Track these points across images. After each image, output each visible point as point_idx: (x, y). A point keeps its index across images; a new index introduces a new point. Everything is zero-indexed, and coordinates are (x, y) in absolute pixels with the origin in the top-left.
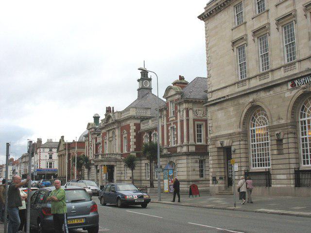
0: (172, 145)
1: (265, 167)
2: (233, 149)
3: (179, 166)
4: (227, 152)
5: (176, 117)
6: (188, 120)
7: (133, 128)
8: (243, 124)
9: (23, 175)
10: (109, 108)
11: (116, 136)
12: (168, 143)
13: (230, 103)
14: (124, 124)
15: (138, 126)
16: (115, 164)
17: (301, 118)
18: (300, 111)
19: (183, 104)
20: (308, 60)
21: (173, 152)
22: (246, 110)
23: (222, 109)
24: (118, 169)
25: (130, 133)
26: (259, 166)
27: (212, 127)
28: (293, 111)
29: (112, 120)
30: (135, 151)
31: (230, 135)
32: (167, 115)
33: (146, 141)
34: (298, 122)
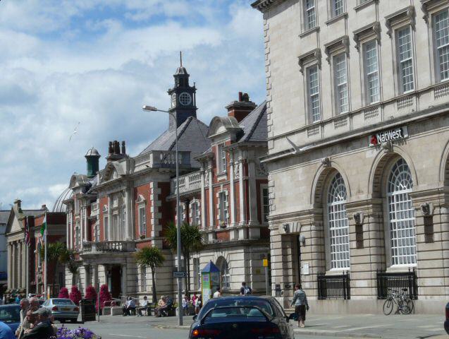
1: (407, 265)
2: (302, 236)
4: (292, 241)
10: (117, 144)
18: (388, 181)
19: (238, 152)
27: (274, 198)
30: (160, 236)
31: (298, 214)
34: (385, 198)
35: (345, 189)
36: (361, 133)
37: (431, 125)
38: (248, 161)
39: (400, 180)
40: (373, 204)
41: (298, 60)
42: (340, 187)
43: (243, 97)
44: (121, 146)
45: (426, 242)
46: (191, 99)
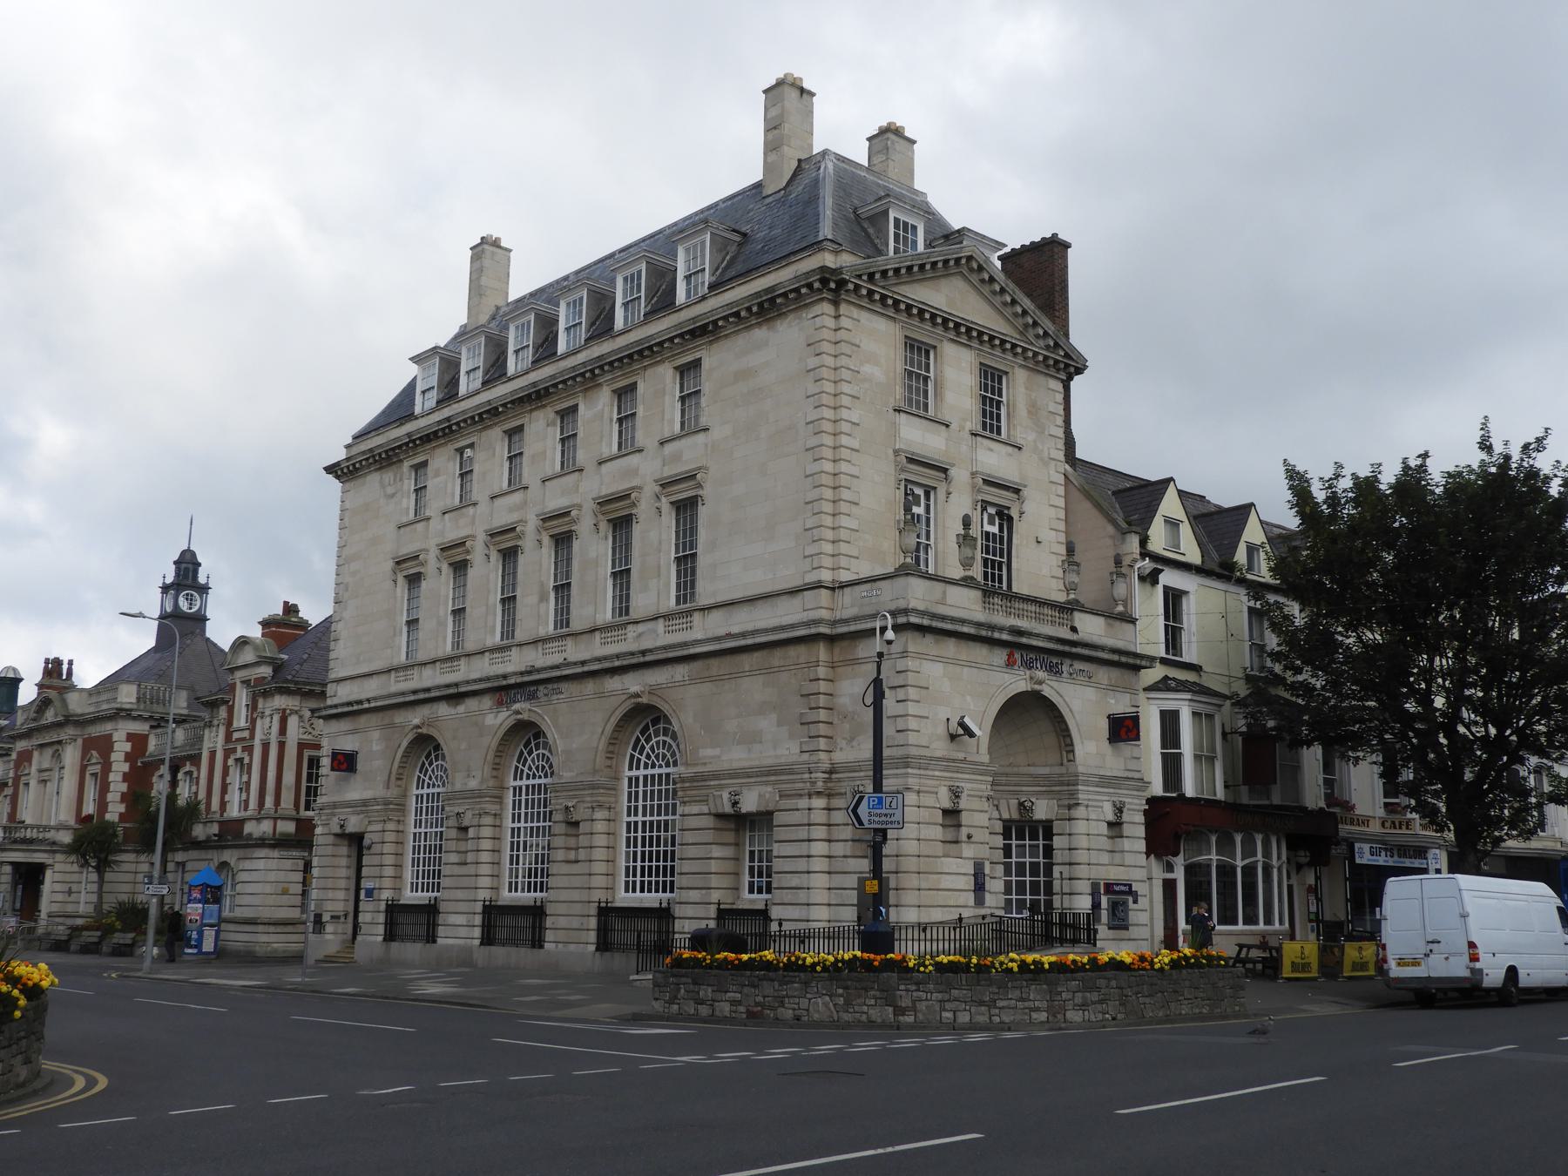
0: (234, 812)
1: (532, 894)
3: (242, 876)
5: (252, 730)
6: (282, 745)
7: (122, 747)
8: (398, 779)
9: (82, 866)
10: (58, 663)
11: (63, 768)
12: (223, 805)
13: (374, 719)
14: (97, 730)
15: (138, 741)
16: (49, 862)
17: (631, 769)
18: (630, 751)
20: (532, 645)
21: (231, 834)
22: (405, 744)
23: (703, 680)
24: (58, 877)
25: (110, 764)
26: (642, 891)
28: (497, 760)
29: (56, 715)
31: (365, 803)
32: (229, 722)
33: (160, 786)
38: (288, 711)
39: (653, 752)
42: (437, 766)
44: (65, 667)
46: (198, 605)
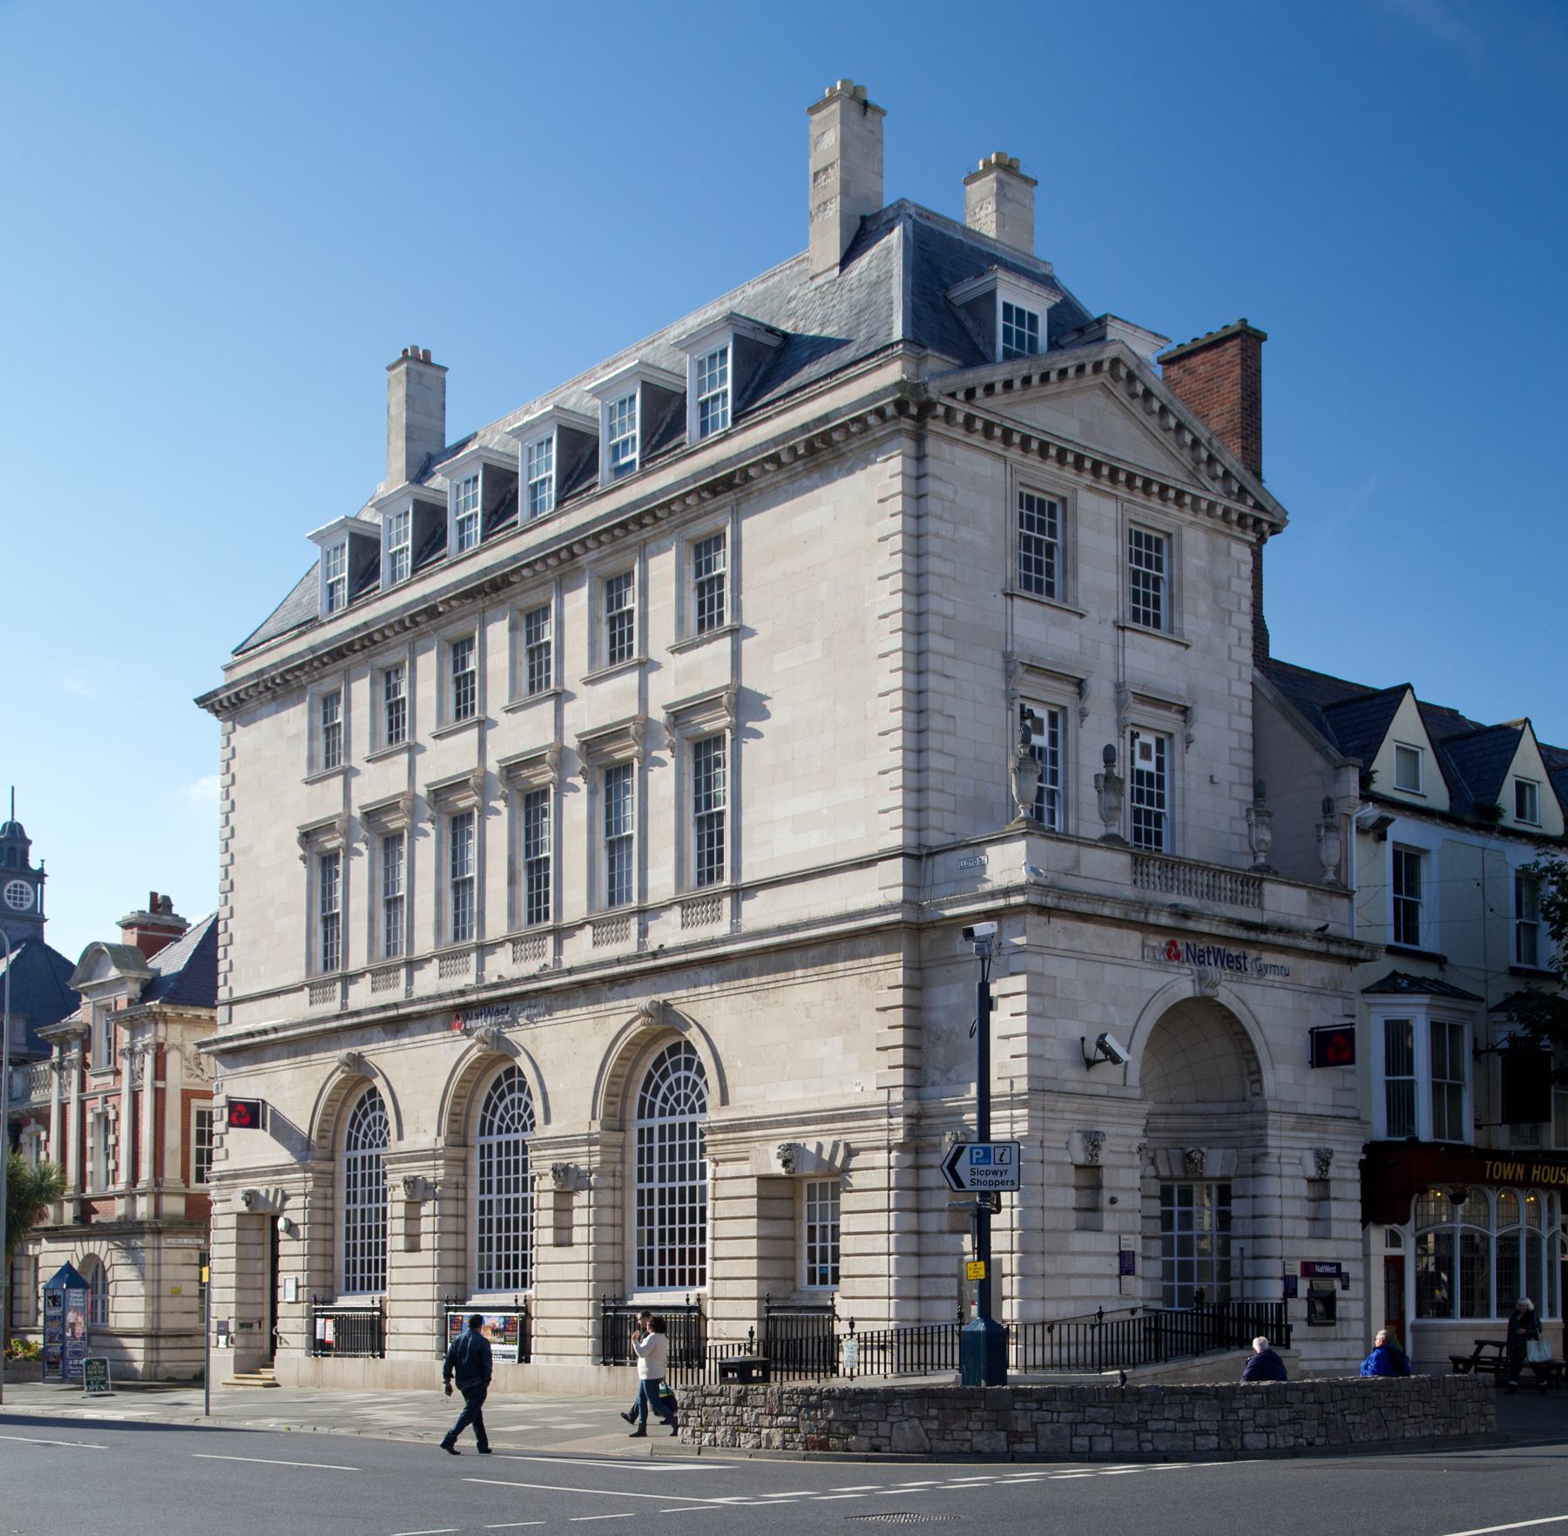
35: (387, 1123)
36: (430, 1006)
37: (582, 999)
40: (447, 1159)
41: (297, 833)
43: (160, 904)
45: (407, 1251)
